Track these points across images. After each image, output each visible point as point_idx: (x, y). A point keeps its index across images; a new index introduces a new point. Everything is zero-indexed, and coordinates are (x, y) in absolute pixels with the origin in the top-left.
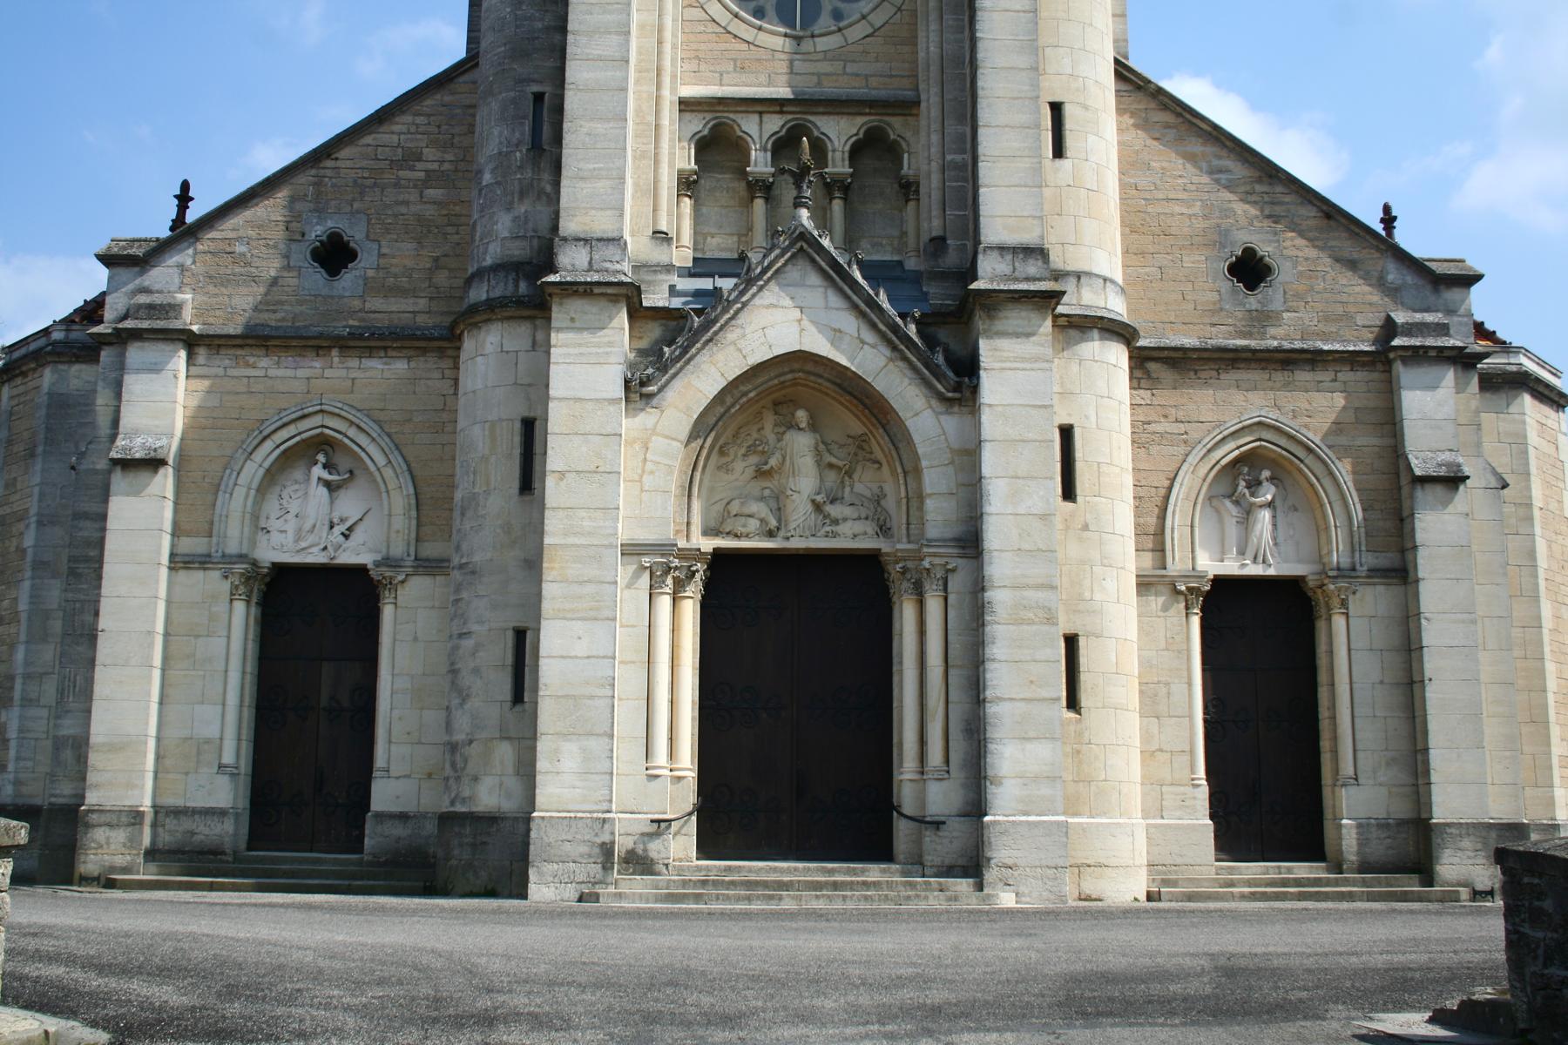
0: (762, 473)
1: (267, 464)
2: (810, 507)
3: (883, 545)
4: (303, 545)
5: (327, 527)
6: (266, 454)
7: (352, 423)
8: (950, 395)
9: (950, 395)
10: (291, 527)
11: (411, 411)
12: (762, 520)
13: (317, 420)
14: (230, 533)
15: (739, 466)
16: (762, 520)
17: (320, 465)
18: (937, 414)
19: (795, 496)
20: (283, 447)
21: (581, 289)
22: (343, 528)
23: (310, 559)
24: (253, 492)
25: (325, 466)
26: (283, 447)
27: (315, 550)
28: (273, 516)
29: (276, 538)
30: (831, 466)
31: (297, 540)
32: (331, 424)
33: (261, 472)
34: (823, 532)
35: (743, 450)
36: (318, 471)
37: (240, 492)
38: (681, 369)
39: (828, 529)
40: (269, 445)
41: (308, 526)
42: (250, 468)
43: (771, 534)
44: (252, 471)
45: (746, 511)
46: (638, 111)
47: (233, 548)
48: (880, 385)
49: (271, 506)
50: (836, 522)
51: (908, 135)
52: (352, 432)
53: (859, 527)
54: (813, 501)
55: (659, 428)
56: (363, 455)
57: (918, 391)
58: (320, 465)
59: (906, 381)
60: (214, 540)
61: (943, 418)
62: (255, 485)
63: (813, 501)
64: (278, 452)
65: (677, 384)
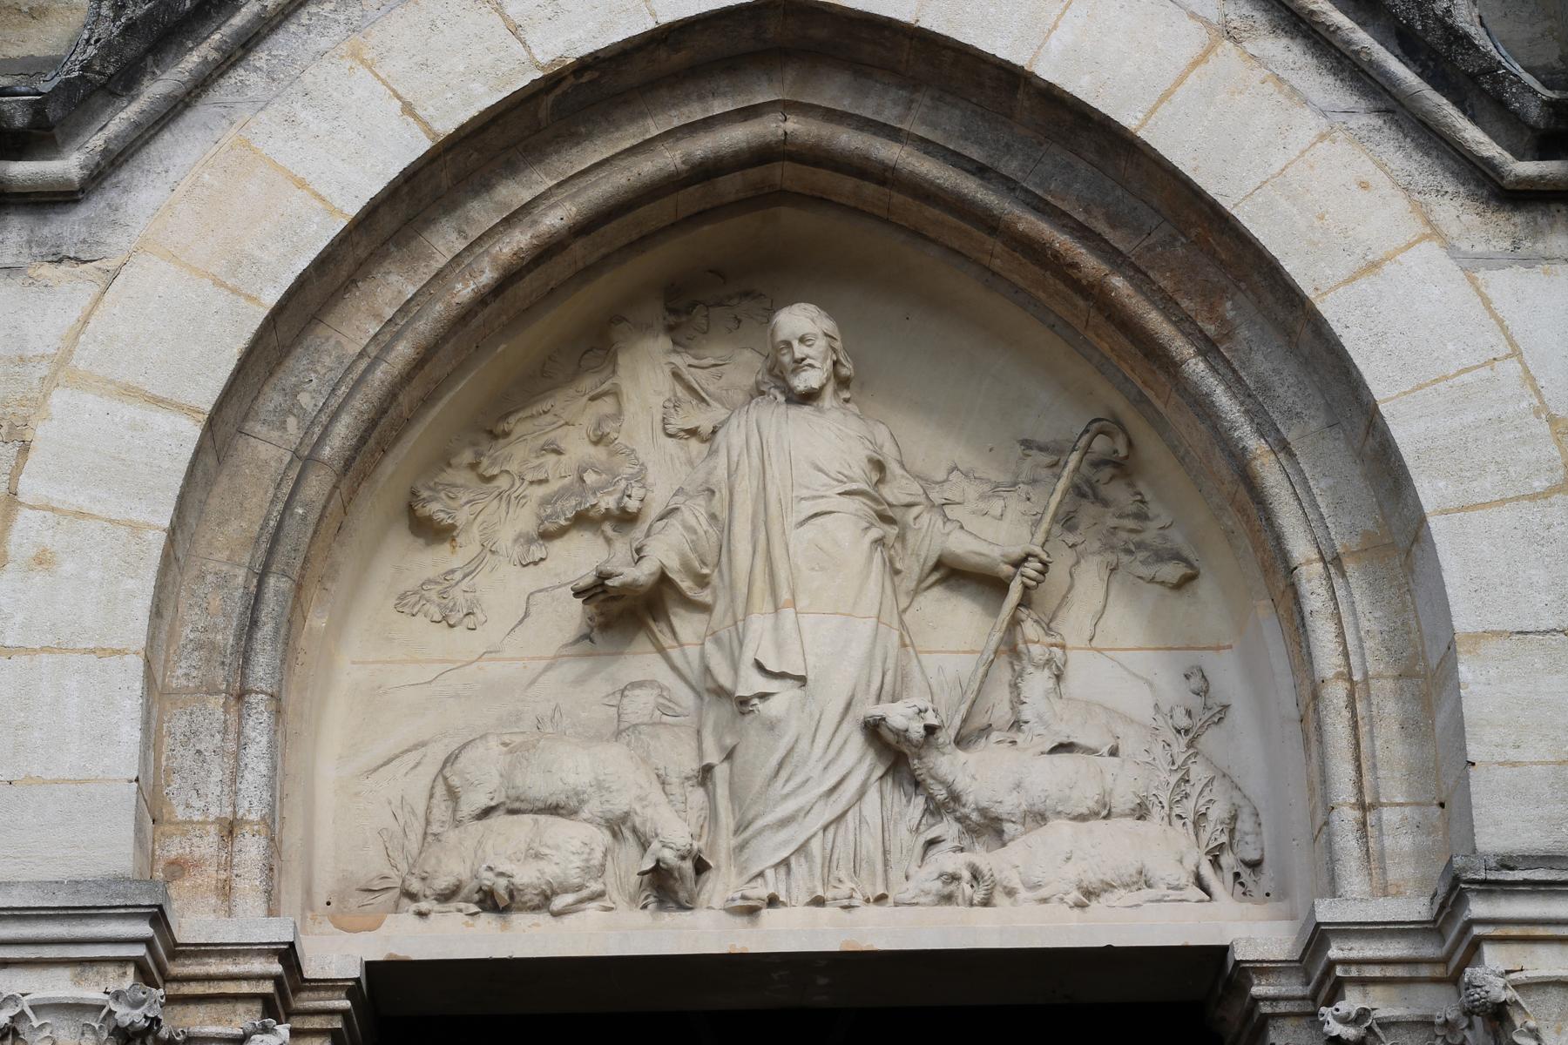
0: (624, 612)
2: (856, 757)
3: (1254, 932)
8: (1528, 168)
9: (1528, 168)
12: (617, 826)
15: (503, 587)
16: (617, 826)
18: (1471, 264)
19: (784, 698)
21: (210, 460)
30: (953, 574)
34: (926, 878)
35: (524, 519)
38: (202, 84)
39: (947, 860)
43: (664, 887)
45: (538, 785)
48: (1179, 140)
50: (989, 828)
51: (723, 869)
53: (1114, 847)
54: (874, 730)
55: (80, 361)
57: (1366, 167)
59: (1307, 125)
61: (1504, 283)
63: (874, 730)
65: (184, 153)
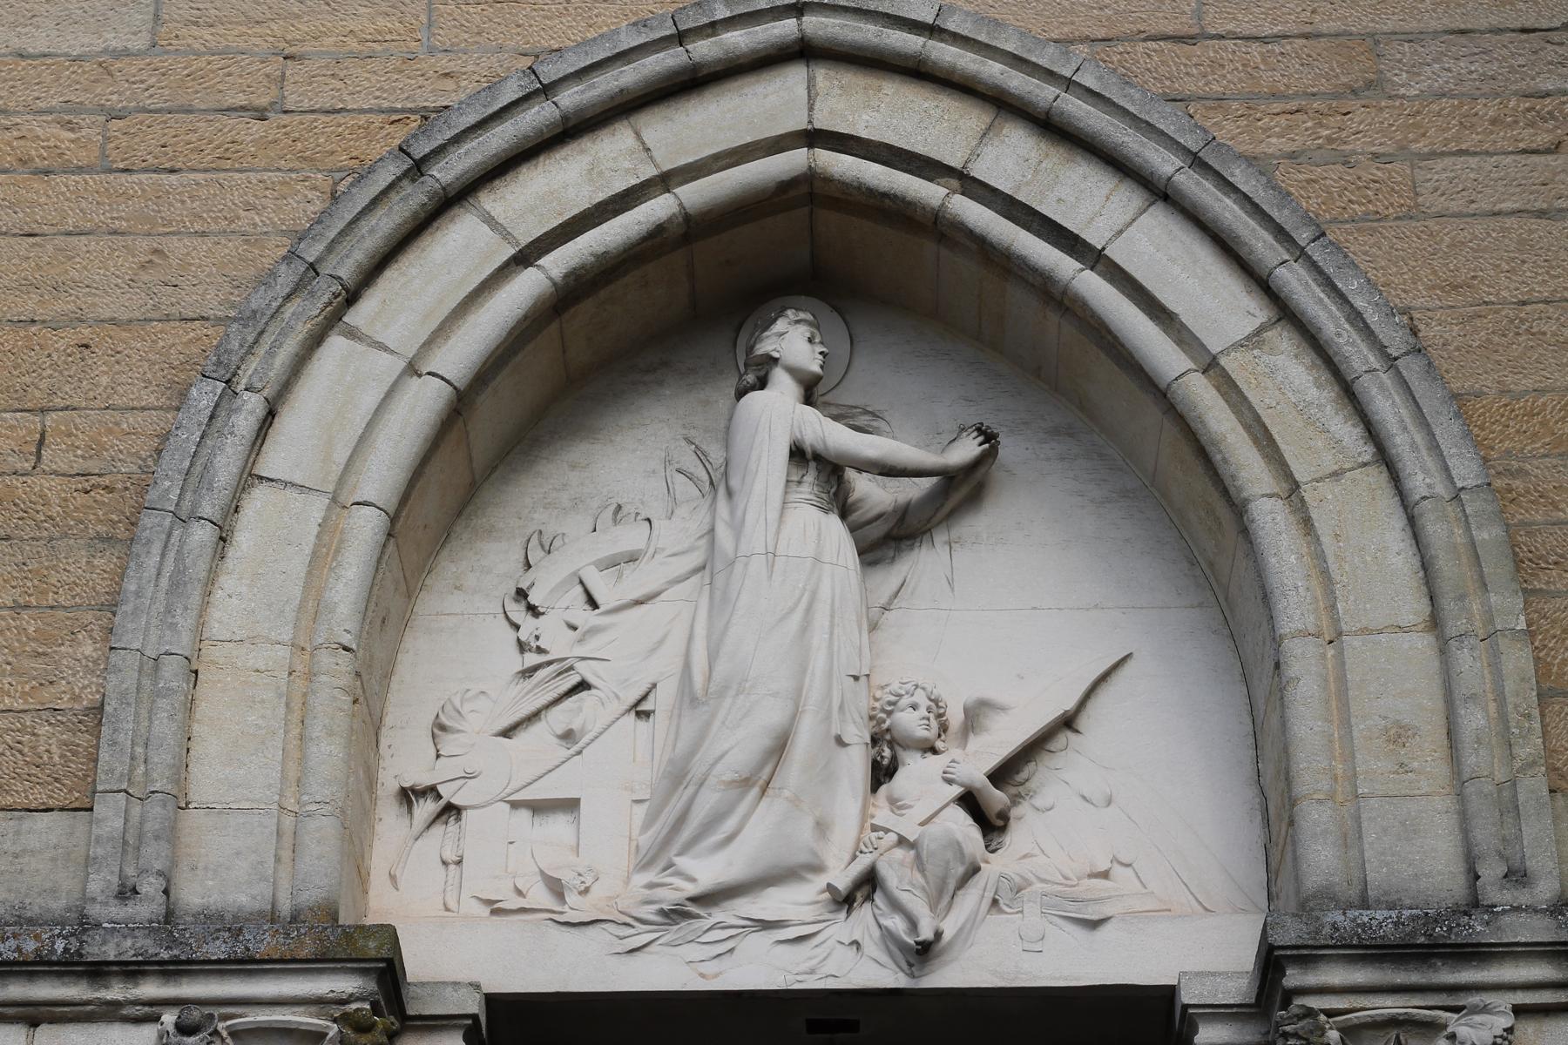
1: (460, 355)
4: (707, 870)
5: (856, 762)
6: (454, 297)
7: (1003, 104)
10: (616, 770)
11: (1373, 40)
13: (778, 101)
14: (209, 779)
17: (783, 388)
20: (559, 262)
22: (975, 761)
23: (758, 967)
24: (366, 527)
25: (810, 391)
26: (559, 262)
27: (793, 902)
28: (480, 719)
29: (501, 849)
31: (669, 840)
32: (864, 125)
33: (423, 402)
36: (776, 415)
37: (274, 530)
40: (463, 246)
41: (736, 744)
42: (343, 380)
44: (365, 402)
46: (311, 1015)
47: (226, 871)
49: (463, 654)
52: (1012, 159)
56: (1093, 287)
58: (783, 388)
60: (110, 815)
62: (382, 474)
64: (527, 287)
